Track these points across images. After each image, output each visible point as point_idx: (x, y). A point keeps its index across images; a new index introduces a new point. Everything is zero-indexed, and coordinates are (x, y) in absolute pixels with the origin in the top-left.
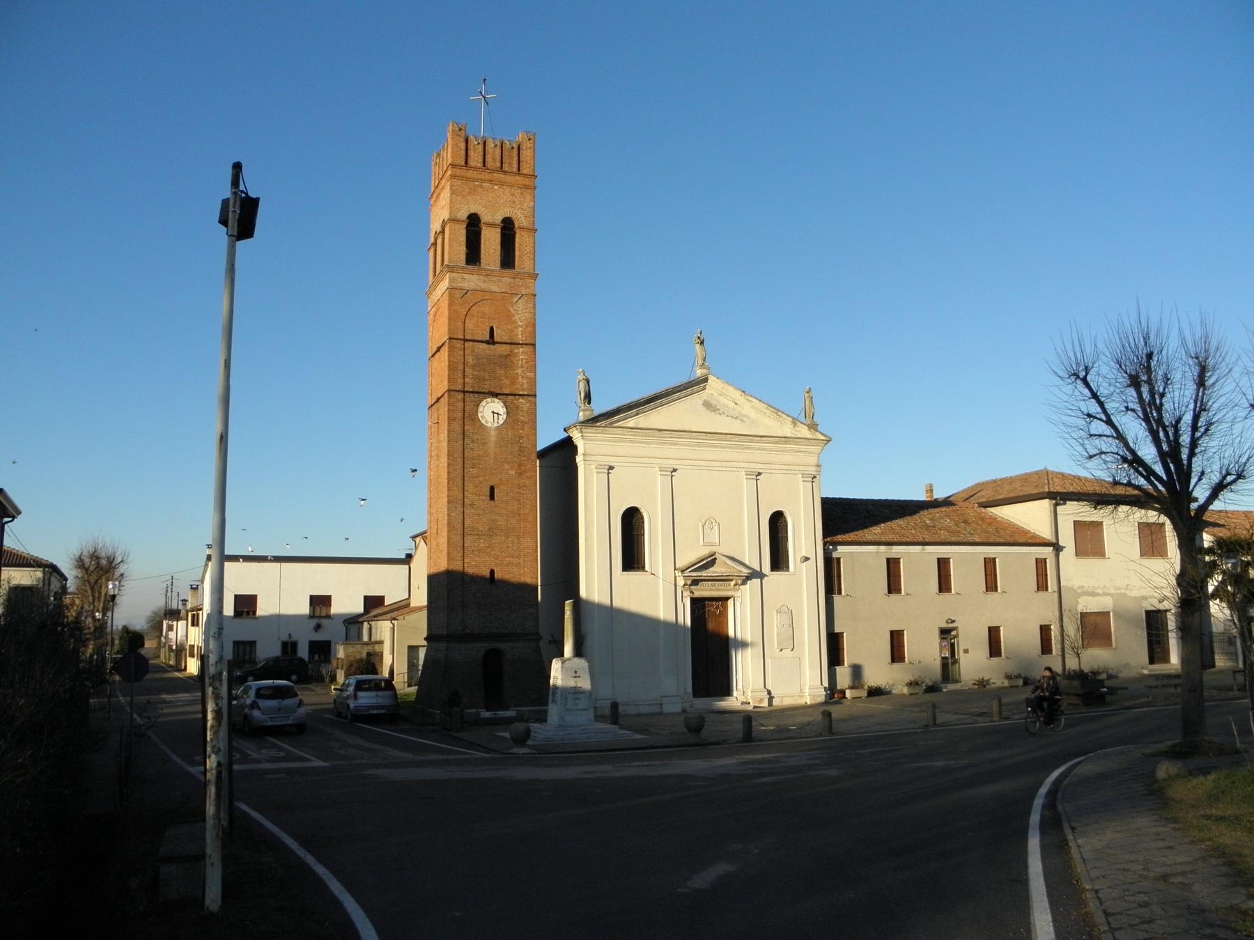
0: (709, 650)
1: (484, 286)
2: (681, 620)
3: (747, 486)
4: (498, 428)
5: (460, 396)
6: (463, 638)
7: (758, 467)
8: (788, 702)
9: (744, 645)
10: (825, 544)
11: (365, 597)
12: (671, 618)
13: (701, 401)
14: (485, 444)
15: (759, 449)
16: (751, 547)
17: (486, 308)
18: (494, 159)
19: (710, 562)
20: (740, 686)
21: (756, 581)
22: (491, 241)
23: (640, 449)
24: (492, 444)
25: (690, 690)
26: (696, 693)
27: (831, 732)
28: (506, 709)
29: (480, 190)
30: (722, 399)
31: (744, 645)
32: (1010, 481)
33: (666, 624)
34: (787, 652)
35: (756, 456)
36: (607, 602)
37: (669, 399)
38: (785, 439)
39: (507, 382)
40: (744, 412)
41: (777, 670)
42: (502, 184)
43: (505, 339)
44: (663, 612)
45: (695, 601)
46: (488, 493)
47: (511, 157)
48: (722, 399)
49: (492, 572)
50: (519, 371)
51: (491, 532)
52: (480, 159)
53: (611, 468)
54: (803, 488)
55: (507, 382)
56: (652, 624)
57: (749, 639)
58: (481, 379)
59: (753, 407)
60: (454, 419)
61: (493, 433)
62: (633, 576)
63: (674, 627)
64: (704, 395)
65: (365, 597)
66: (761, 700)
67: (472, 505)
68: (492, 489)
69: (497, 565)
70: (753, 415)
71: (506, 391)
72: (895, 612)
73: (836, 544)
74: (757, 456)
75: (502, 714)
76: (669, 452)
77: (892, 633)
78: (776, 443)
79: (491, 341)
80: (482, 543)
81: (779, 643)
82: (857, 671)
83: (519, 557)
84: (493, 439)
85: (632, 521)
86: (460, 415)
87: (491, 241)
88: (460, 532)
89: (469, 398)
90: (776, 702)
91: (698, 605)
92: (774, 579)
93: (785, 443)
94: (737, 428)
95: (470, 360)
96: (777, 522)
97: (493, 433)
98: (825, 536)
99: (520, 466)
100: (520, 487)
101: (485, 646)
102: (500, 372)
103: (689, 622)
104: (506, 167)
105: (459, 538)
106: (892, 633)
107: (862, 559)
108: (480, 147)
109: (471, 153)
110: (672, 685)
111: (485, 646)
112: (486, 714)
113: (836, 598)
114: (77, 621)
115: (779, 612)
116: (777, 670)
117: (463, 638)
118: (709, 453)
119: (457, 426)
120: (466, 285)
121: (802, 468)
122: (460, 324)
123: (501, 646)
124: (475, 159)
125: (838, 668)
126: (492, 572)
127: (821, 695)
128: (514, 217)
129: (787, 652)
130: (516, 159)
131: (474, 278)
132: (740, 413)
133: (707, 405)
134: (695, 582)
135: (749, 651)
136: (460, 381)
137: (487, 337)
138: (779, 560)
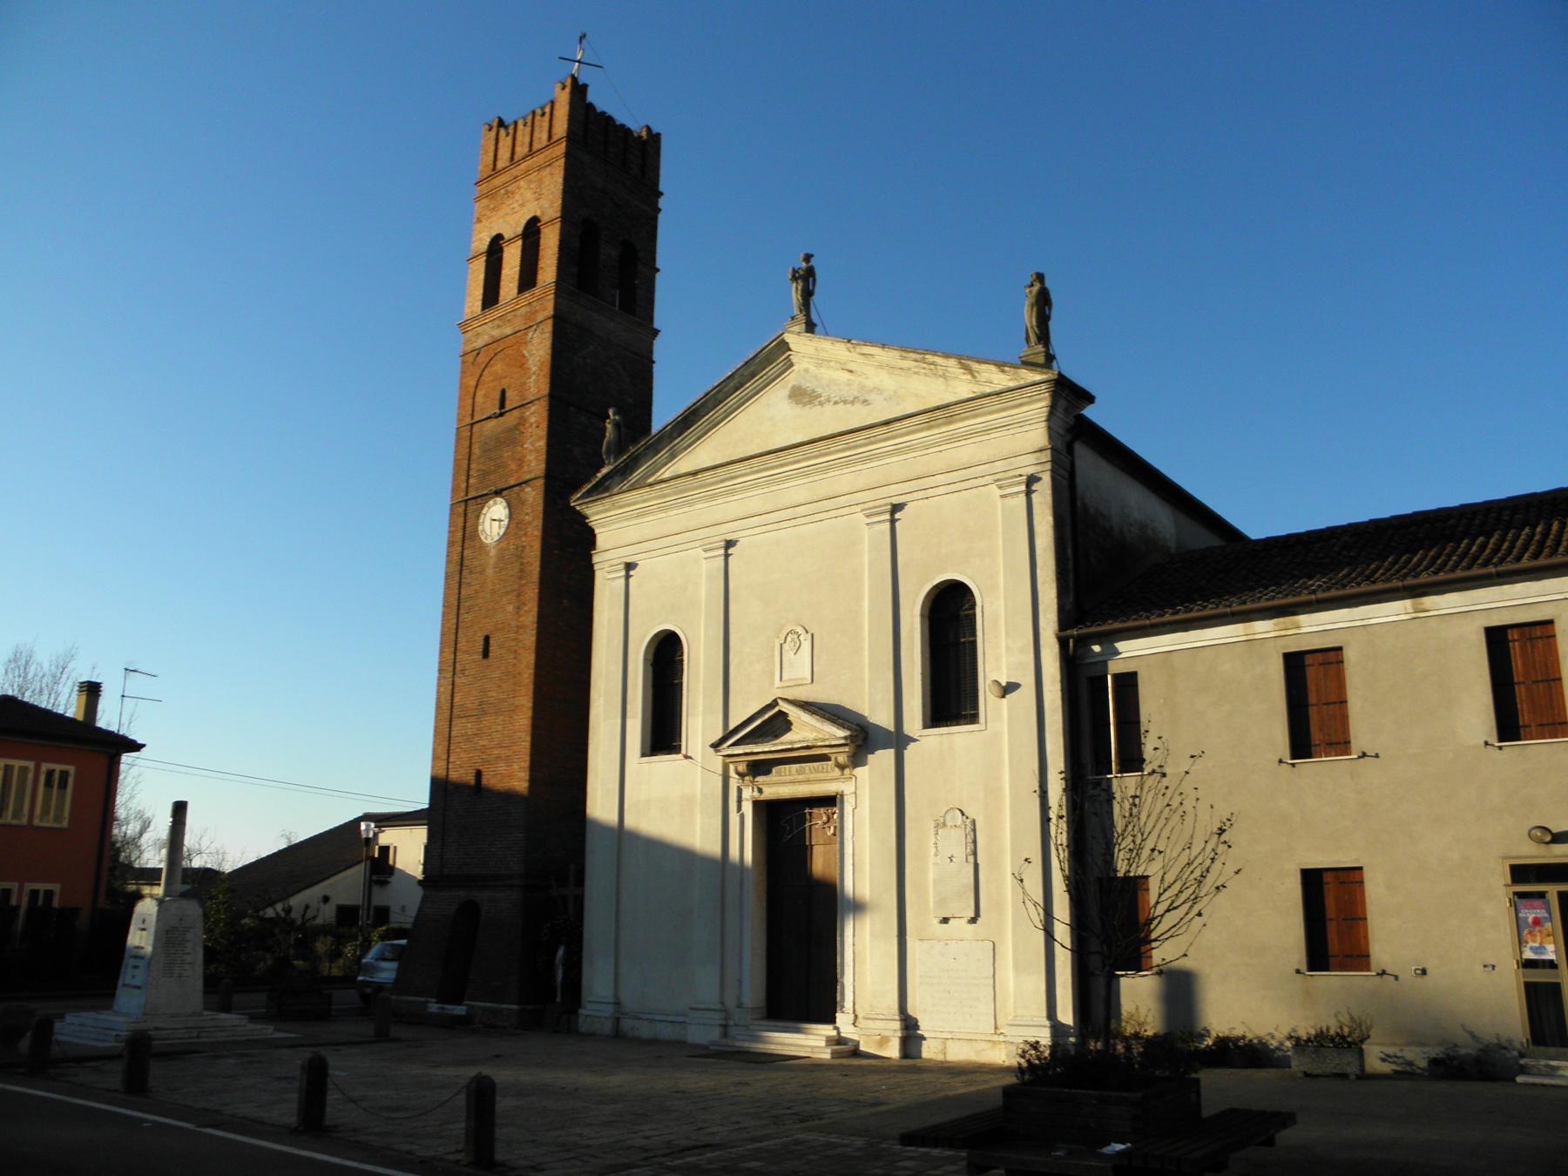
0: (793, 916)
1: (496, 333)
7: (894, 494)
8: (959, 1053)
12: (713, 847)
13: (786, 392)
14: (482, 572)
19: (773, 724)
20: (848, 1004)
24: (490, 571)
31: (857, 907)
32: (452, 524)
34: (959, 926)
35: (886, 470)
40: (870, 384)
41: (955, 972)
44: (700, 835)
48: (827, 374)
49: (479, 774)
53: (630, 567)
59: (880, 366)
63: (722, 864)
64: (791, 379)
66: (884, 1041)
72: (1321, 818)
73: (1109, 638)
74: (896, 466)
77: (1312, 880)
81: (941, 902)
84: (492, 562)
85: (666, 655)
90: (929, 1051)
92: (935, 748)
93: (950, 420)
96: (950, 611)
97: (493, 553)
106: (1312, 880)
107: (1203, 676)
112: (434, 1007)
114: (1028, 1061)
118: (797, 491)
121: (1000, 466)
126: (479, 774)
129: (959, 926)
132: (862, 387)
133: (800, 395)
134: (759, 768)
138: (952, 696)
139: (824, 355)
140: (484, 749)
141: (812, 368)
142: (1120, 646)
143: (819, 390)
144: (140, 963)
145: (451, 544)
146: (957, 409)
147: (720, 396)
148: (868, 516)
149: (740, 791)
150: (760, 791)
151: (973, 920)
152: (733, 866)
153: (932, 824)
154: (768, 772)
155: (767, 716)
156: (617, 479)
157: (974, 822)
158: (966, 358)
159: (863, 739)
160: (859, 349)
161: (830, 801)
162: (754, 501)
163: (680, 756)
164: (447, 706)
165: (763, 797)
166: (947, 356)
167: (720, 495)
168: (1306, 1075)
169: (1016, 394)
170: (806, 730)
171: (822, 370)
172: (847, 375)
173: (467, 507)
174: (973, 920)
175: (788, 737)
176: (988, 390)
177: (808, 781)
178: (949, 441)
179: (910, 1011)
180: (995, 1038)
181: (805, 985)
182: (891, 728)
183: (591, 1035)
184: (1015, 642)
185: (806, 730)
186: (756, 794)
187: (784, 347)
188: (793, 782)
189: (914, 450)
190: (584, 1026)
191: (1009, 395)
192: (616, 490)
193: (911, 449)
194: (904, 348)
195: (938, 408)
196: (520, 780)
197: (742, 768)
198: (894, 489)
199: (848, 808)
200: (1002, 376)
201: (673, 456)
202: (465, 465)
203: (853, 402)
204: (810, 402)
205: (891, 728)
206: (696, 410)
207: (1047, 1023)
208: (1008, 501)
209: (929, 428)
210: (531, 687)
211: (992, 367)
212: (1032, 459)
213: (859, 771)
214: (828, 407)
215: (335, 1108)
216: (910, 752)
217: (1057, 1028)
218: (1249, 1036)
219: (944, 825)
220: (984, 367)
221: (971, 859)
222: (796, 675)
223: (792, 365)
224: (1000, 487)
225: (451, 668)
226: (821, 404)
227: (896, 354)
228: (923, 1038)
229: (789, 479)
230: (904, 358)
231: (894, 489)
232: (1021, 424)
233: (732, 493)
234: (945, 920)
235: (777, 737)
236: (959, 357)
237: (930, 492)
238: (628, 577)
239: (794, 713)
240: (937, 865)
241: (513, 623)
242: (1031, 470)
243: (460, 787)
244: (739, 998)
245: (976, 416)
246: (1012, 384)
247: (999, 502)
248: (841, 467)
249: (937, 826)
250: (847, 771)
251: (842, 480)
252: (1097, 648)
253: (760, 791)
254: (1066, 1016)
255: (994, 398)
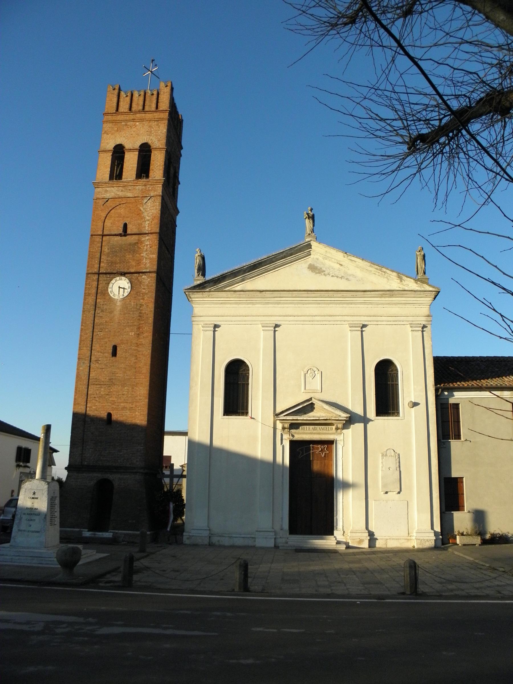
0: (309, 487)
1: (121, 194)
2: (279, 460)
3: (352, 338)
4: (124, 299)
5: (96, 277)
6: (91, 468)
7: (363, 320)
8: (393, 544)
9: (346, 485)
10: (437, 390)
11: (224, 415)
12: (269, 457)
13: (307, 266)
14: (111, 312)
15: (364, 303)
16: (356, 392)
17: (122, 211)
18: (138, 104)
19: (308, 407)
21: (359, 427)
22: (131, 161)
23: (243, 309)
24: (117, 313)
25: (286, 526)
26: (293, 530)
27: (245, 588)
28: (106, 531)
29: (125, 127)
30: (327, 262)
31: (346, 485)
33: (263, 463)
34: (393, 495)
35: (361, 310)
36: (207, 441)
37: (273, 265)
38: (391, 292)
39: (133, 263)
40: (350, 272)
41: (385, 509)
42: (141, 120)
43: (135, 231)
44: (261, 451)
45: (294, 444)
46: (111, 351)
47: (151, 101)
48: (327, 262)
50: (144, 254)
51: (111, 382)
52: (128, 106)
53: (216, 326)
54: (413, 338)
55: (133, 263)
56: (250, 463)
57: (350, 478)
58: (112, 263)
59: (357, 267)
60: (89, 294)
61: (119, 304)
62: (235, 420)
64: (309, 260)
65: (224, 415)
66: (361, 541)
67: (97, 361)
68: (115, 348)
69: (113, 409)
70: (359, 273)
71: (132, 270)
73: (452, 390)
74: (363, 310)
75: (100, 534)
76: (273, 311)
78: (381, 296)
79: (125, 232)
80: (103, 391)
82: (479, 517)
83: (132, 403)
86: (94, 291)
87: (131, 161)
88: (86, 382)
89: (102, 278)
90: (379, 544)
91: (298, 448)
92: (380, 425)
93: (391, 296)
94: (343, 285)
95: (106, 249)
97: (119, 304)
98: (436, 384)
99: (139, 328)
100: (137, 345)
101: (99, 476)
102: (129, 256)
103: (287, 462)
104: (147, 109)
105: (84, 387)
108: (128, 99)
109: (121, 104)
110: (268, 518)
111: (99, 476)
112: (87, 534)
113: (454, 444)
115: (384, 455)
116: (385, 509)
117: (91, 468)
118: (312, 309)
119: (91, 300)
120: (108, 195)
121: (411, 319)
122: (100, 224)
123: (110, 477)
124: (124, 106)
125: (456, 515)
127: (428, 539)
128: (150, 142)
129: (393, 495)
130: (155, 101)
131: (115, 190)
133: (312, 268)
134: (294, 426)
135: (350, 493)
136: (97, 266)
137: (121, 231)
139: (329, 255)
140: (113, 403)
141: (321, 259)
142: (455, 393)
143: (324, 269)
144: (37, 518)
145: (87, 295)
146: (396, 293)
147: (274, 260)
148: (350, 327)
149: (282, 435)
150: (293, 436)
151: (399, 493)
152: (279, 465)
153: (381, 455)
154: (298, 428)
155: (305, 405)
156: (211, 284)
157: (399, 455)
158: (400, 275)
159: (352, 419)
160: (349, 257)
161: (330, 443)
162: (290, 309)
163: (248, 417)
164: (85, 378)
165: (295, 439)
166: (393, 271)
167: (272, 303)
168: (464, 545)
169: (422, 293)
170: (320, 413)
171: (326, 261)
172: (338, 266)
173: (100, 276)
174: (399, 493)
175: (311, 414)
176: (407, 289)
177: (319, 434)
178: (389, 304)
179: (370, 529)
180: (409, 538)
181: (323, 520)
182: (362, 415)
183: (185, 544)
184: (415, 385)
185: (320, 413)
186: (291, 437)
187: (309, 246)
188: (311, 433)
189: (372, 304)
190: (186, 541)
191: (419, 293)
192: (208, 290)
193: (371, 303)
194: (373, 263)
195: (389, 291)
196: (142, 420)
197: (287, 426)
198: (363, 318)
199: (340, 447)
200: (415, 284)
201: (243, 280)
202: (96, 255)
203: (341, 278)
204: (319, 273)
205: (362, 415)
206: (261, 263)
207: (367, 531)
208: (414, 333)
209: (380, 297)
210: (148, 375)
211: (412, 280)
212: (424, 319)
213: (345, 431)
214: (329, 278)
215: (421, 588)
216: (369, 425)
217: (436, 533)
218: (501, 533)
219: (386, 455)
220: (409, 279)
221: (398, 469)
222: (312, 389)
223: (310, 255)
224: (411, 327)
225: (87, 358)
226: (324, 275)
227: (369, 264)
228: (376, 539)
229: (309, 304)
230: (371, 266)
231: (363, 318)
232: (420, 304)
233: (278, 303)
234: (386, 493)
235: (305, 413)
236: (398, 273)
237: (379, 323)
238: (214, 331)
239: (318, 405)
240: (381, 470)
241: (134, 341)
242: (424, 323)
243: (95, 420)
244: (282, 525)
245: (402, 297)
246: (419, 289)
247: (411, 333)
248: (336, 304)
249: (383, 455)
250: (339, 431)
251: (346, 310)
252: (446, 393)
253: (293, 436)
254: (438, 529)
255: (413, 292)
